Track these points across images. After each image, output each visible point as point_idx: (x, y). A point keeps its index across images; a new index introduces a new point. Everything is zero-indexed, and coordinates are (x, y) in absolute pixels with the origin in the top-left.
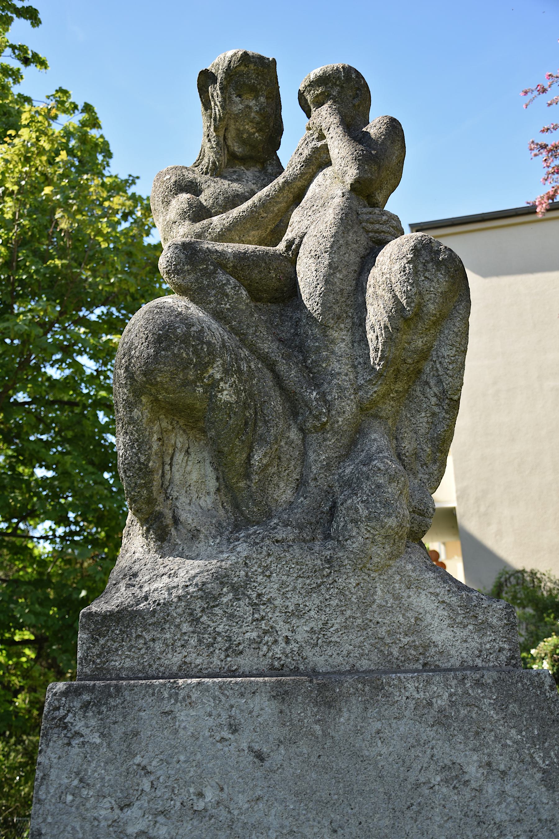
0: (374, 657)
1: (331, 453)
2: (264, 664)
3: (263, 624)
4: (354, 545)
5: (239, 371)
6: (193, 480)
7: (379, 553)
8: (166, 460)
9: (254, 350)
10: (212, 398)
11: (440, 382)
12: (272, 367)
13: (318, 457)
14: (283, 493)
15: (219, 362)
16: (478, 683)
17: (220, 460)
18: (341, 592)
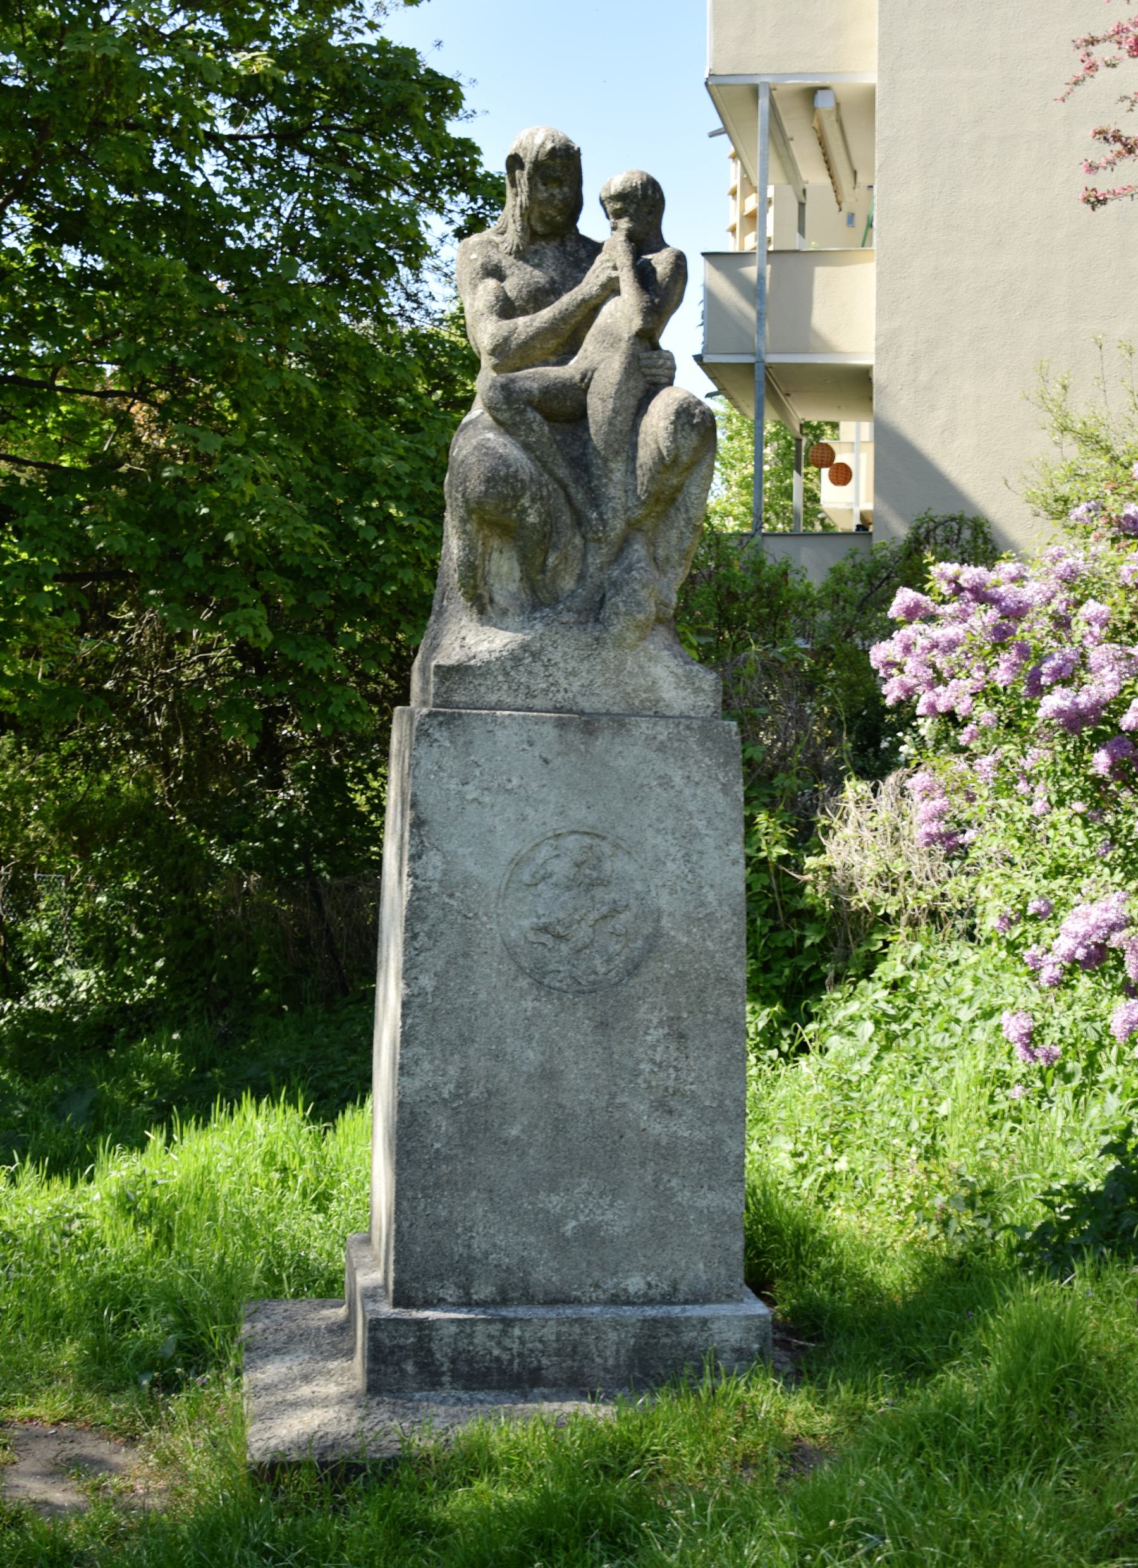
0: (623, 705)
1: (604, 559)
2: (550, 705)
3: (551, 679)
4: (614, 630)
5: (542, 498)
6: (504, 571)
7: (631, 637)
8: (486, 556)
9: (551, 473)
10: (522, 520)
11: (687, 511)
12: (564, 488)
13: (595, 560)
14: (568, 583)
15: (528, 494)
16: (688, 728)
17: (524, 560)
18: (604, 661)
